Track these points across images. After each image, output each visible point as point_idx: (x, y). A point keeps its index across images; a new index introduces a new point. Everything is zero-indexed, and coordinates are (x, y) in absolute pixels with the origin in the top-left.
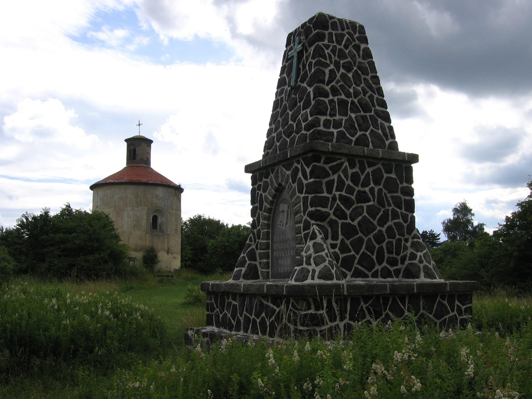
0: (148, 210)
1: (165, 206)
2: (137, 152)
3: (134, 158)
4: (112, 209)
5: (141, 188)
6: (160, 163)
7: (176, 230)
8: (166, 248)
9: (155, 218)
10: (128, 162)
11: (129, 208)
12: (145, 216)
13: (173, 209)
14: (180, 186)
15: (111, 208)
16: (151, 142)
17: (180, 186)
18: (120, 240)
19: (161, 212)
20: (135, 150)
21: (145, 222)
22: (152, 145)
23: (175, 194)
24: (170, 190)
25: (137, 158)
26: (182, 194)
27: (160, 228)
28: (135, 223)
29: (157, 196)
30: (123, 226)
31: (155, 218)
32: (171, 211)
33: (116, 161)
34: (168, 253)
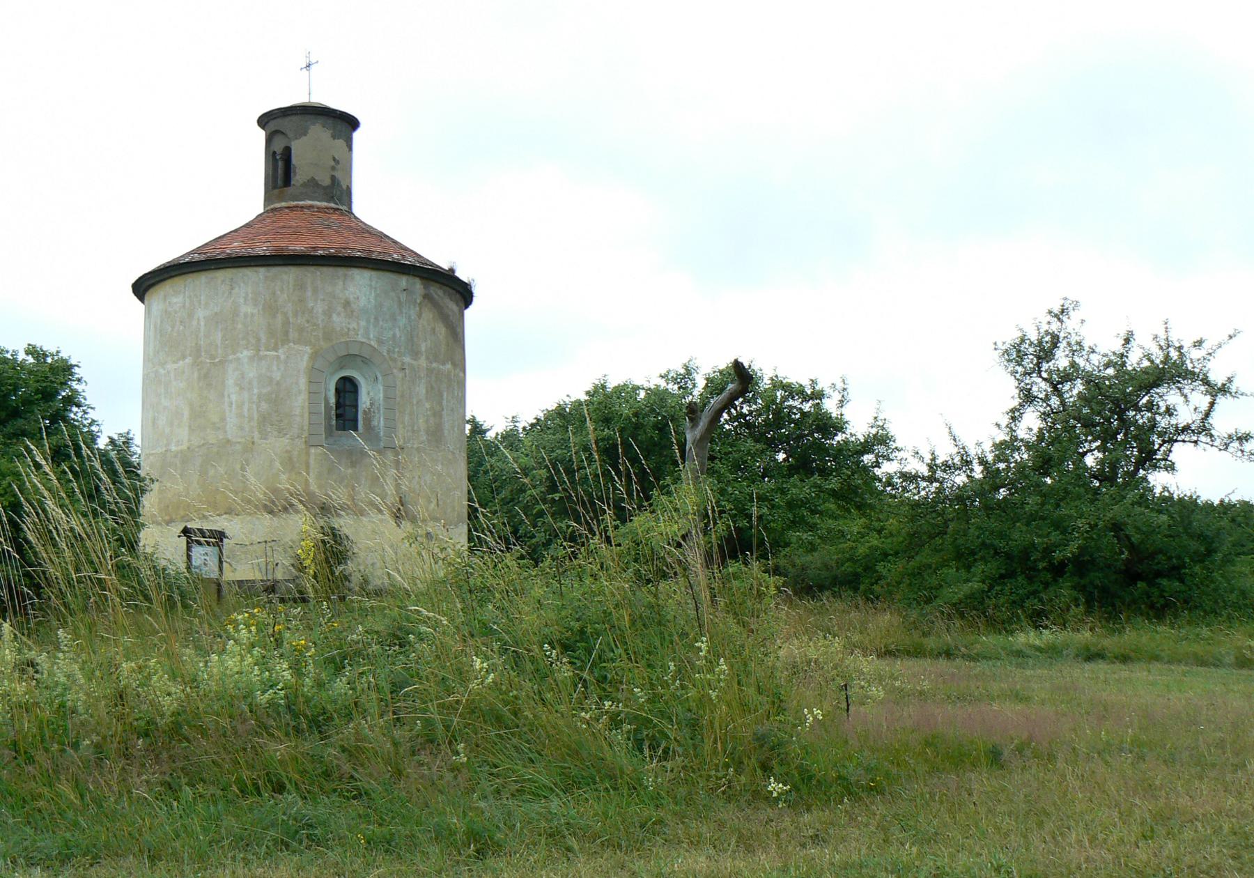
0: (314, 356)
1: (381, 342)
2: (294, 161)
3: (287, 181)
4: (188, 360)
5: (290, 274)
6: (388, 197)
7: (436, 435)
8: (392, 499)
9: (347, 389)
10: (268, 199)
11: (245, 354)
12: (303, 382)
13: (416, 354)
14: (452, 270)
15: (184, 357)
16: (351, 123)
17: (452, 270)
18: (485, 432)
19: (366, 361)
20: (287, 153)
21: (305, 400)
22: (357, 136)
23: (427, 297)
24: (404, 281)
25: (298, 178)
26: (467, 312)
27: (368, 421)
28: (264, 406)
29: (347, 304)
30: (223, 419)
31: (347, 389)
32: (407, 359)
33: (233, 196)
34: (397, 517)
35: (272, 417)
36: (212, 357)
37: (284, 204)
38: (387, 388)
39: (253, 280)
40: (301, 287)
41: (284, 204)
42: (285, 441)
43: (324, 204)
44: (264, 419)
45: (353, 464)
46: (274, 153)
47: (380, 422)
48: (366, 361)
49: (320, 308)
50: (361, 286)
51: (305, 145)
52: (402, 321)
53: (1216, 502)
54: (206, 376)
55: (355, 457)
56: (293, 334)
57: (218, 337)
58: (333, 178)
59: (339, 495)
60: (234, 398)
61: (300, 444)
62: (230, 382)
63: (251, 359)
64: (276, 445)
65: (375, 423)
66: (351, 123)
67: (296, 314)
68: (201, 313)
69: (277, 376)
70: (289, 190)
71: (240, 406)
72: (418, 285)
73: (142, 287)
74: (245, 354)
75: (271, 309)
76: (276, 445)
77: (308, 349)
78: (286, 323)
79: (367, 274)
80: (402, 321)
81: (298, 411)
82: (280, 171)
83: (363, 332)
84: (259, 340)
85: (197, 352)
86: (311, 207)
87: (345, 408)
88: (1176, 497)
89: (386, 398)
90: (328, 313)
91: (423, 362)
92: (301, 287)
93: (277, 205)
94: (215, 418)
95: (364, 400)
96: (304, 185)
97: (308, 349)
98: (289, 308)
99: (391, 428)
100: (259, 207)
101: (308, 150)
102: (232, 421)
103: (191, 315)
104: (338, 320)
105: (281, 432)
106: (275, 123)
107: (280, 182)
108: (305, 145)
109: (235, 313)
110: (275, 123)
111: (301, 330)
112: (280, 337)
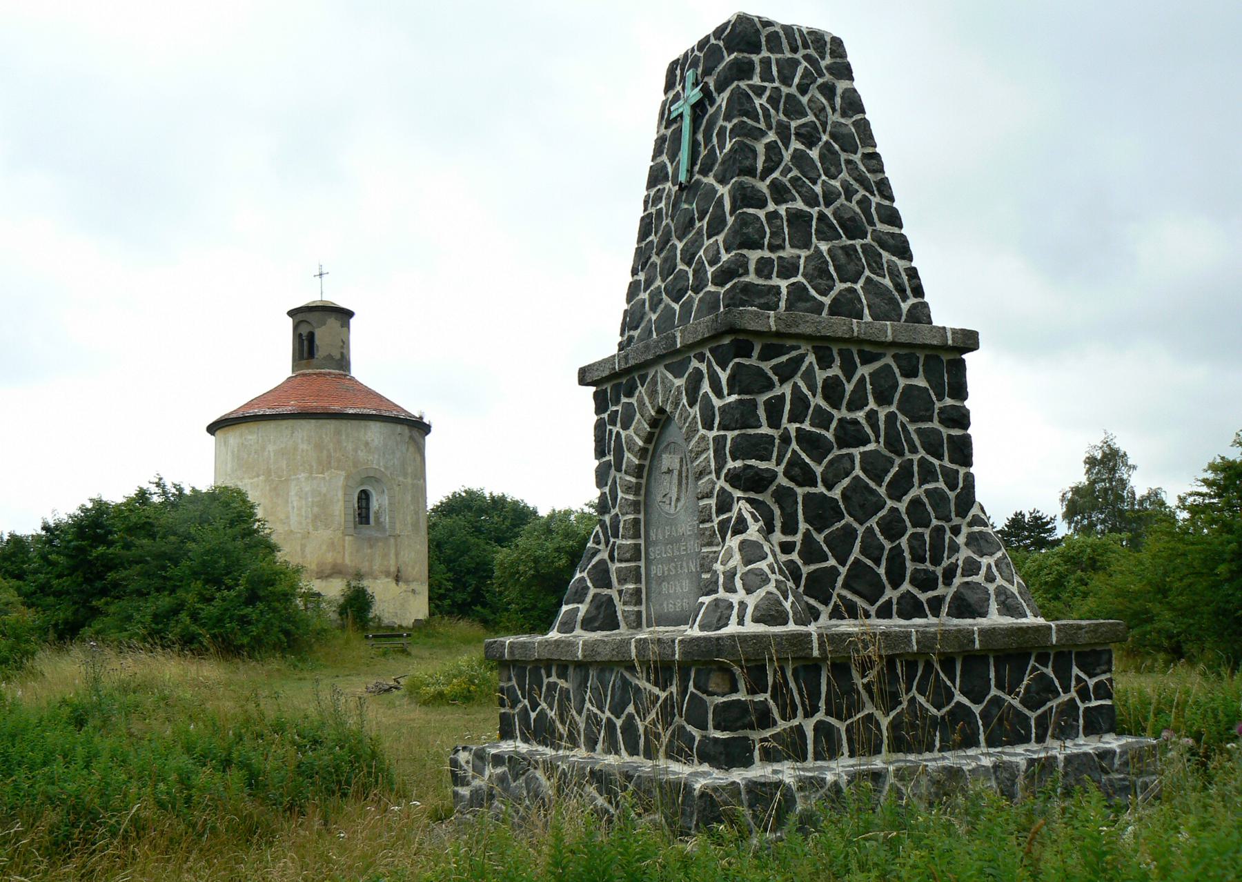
0: (347, 478)
1: (386, 468)
2: (317, 342)
3: (311, 354)
5: (332, 425)
6: (375, 363)
9: (364, 497)
11: (302, 476)
12: (340, 494)
13: (405, 475)
15: (258, 476)
16: (349, 314)
19: (377, 480)
20: (311, 336)
22: (352, 321)
23: (411, 437)
24: (399, 428)
25: (320, 353)
28: (316, 509)
29: (367, 444)
30: (288, 517)
31: (364, 497)
32: (401, 479)
33: (270, 365)
35: (320, 517)
36: (280, 477)
37: (310, 371)
38: (391, 497)
39: (306, 429)
40: (338, 433)
41: (310, 371)
42: (329, 532)
43: (337, 371)
44: (316, 517)
45: (371, 547)
46: (300, 335)
47: (386, 519)
48: (377, 480)
49: (350, 447)
50: (375, 433)
51: (319, 332)
52: (398, 454)
53: (544, 512)
54: (275, 489)
55: (371, 541)
56: (334, 464)
57: (284, 464)
58: (342, 354)
59: (365, 567)
60: (295, 504)
61: (339, 534)
62: (292, 493)
63: (307, 479)
64: (324, 534)
65: (382, 520)
66: (349, 314)
67: (335, 451)
68: (271, 448)
69: (324, 490)
70: (314, 361)
71: (300, 509)
72: (405, 430)
73: (213, 428)
74: (302, 476)
75: (319, 447)
76: (324, 534)
77: (343, 473)
78: (329, 456)
79: (378, 424)
80: (398, 454)
81: (337, 513)
82: (305, 348)
83: (376, 462)
84: (311, 467)
85: (268, 472)
86: (330, 374)
87: (363, 512)
88: (187, 491)
89: (390, 504)
90: (355, 450)
91: (409, 480)
92: (338, 433)
93: (307, 371)
94: (282, 516)
95: (374, 505)
96: (324, 358)
97: (343, 473)
98: (331, 446)
99: (393, 523)
100: (288, 373)
101: (324, 335)
102: (294, 519)
103: (263, 448)
104: (362, 454)
105: (327, 526)
106: (300, 315)
107: (305, 355)
108: (319, 332)
109: (295, 449)
110: (300, 315)
111: (339, 461)
112: (325, 465)
